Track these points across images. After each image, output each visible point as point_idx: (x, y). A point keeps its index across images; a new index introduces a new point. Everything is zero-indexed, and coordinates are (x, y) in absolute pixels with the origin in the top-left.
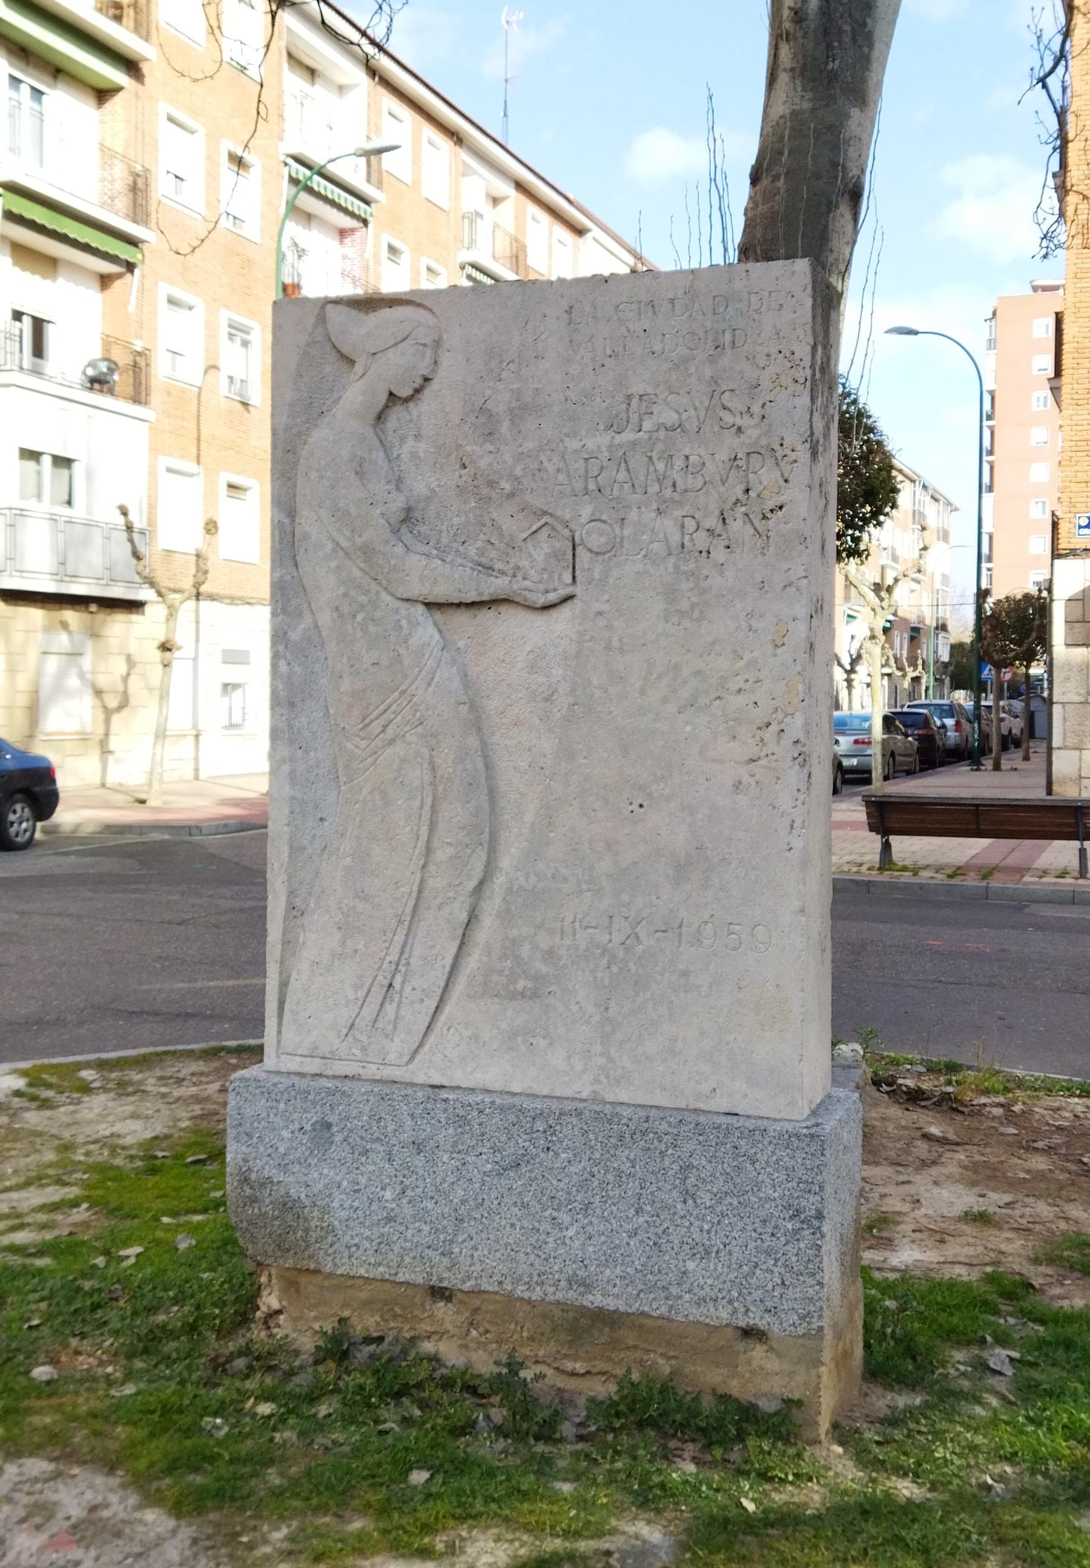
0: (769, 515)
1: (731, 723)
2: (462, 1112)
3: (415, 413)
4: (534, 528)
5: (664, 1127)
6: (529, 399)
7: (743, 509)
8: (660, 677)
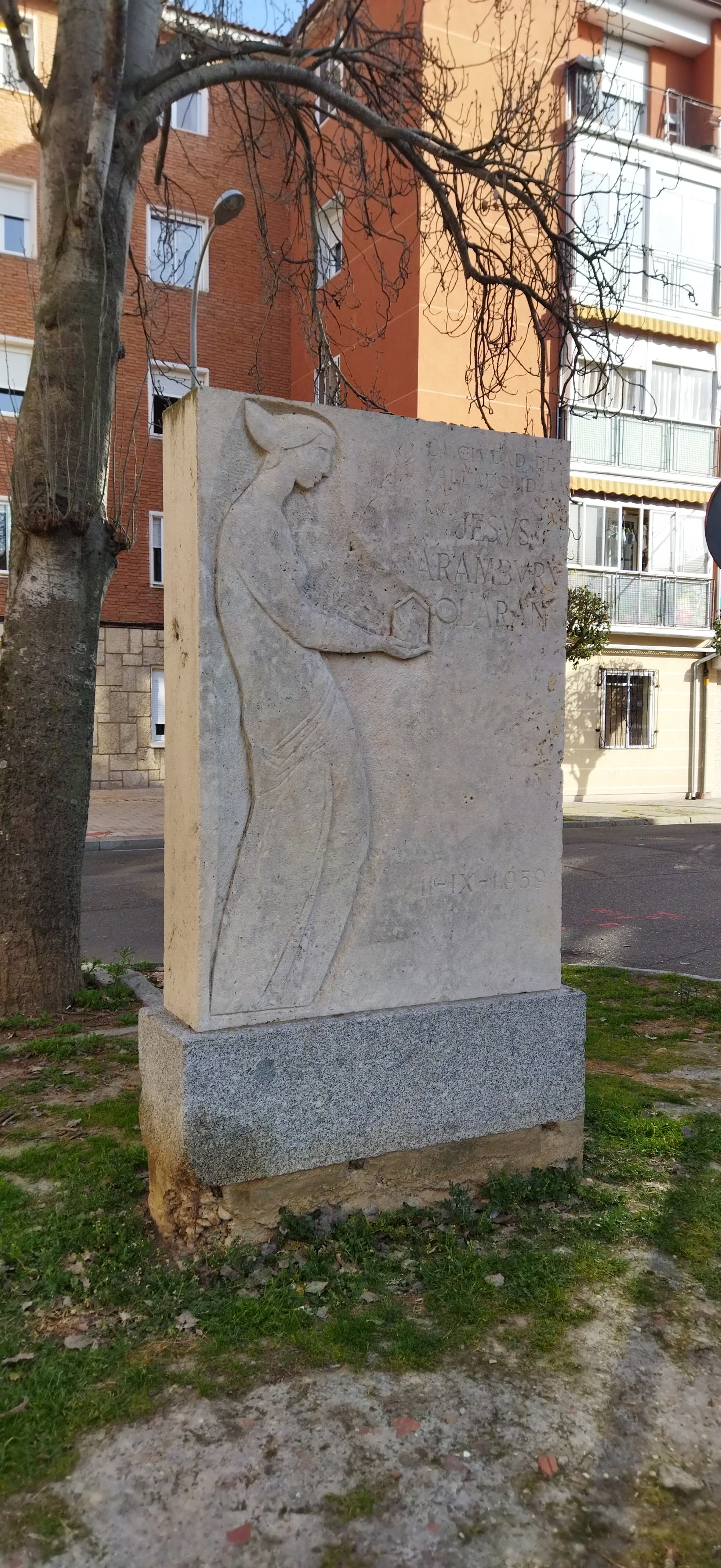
2: (373, 1029)
3: (311, 501)
5: (501, 1008)
6: (402, 505)
7: (531, 600)
8: (484, 710)
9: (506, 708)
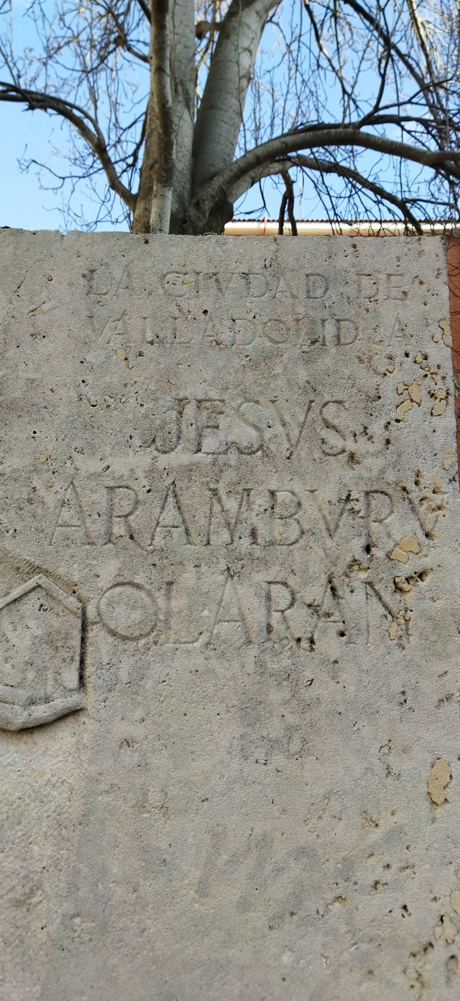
0: (405, 586)
1: (364, 947)
4: (15, 593)
6: (18, 394)
7: (363, 575)
8: (234, 860)
9: (302, 852)
